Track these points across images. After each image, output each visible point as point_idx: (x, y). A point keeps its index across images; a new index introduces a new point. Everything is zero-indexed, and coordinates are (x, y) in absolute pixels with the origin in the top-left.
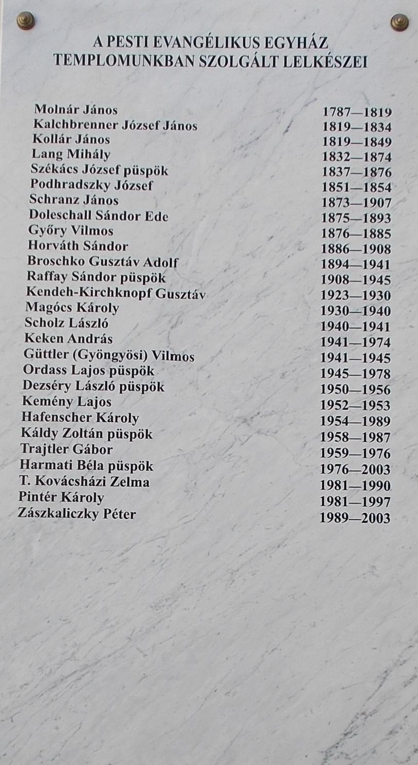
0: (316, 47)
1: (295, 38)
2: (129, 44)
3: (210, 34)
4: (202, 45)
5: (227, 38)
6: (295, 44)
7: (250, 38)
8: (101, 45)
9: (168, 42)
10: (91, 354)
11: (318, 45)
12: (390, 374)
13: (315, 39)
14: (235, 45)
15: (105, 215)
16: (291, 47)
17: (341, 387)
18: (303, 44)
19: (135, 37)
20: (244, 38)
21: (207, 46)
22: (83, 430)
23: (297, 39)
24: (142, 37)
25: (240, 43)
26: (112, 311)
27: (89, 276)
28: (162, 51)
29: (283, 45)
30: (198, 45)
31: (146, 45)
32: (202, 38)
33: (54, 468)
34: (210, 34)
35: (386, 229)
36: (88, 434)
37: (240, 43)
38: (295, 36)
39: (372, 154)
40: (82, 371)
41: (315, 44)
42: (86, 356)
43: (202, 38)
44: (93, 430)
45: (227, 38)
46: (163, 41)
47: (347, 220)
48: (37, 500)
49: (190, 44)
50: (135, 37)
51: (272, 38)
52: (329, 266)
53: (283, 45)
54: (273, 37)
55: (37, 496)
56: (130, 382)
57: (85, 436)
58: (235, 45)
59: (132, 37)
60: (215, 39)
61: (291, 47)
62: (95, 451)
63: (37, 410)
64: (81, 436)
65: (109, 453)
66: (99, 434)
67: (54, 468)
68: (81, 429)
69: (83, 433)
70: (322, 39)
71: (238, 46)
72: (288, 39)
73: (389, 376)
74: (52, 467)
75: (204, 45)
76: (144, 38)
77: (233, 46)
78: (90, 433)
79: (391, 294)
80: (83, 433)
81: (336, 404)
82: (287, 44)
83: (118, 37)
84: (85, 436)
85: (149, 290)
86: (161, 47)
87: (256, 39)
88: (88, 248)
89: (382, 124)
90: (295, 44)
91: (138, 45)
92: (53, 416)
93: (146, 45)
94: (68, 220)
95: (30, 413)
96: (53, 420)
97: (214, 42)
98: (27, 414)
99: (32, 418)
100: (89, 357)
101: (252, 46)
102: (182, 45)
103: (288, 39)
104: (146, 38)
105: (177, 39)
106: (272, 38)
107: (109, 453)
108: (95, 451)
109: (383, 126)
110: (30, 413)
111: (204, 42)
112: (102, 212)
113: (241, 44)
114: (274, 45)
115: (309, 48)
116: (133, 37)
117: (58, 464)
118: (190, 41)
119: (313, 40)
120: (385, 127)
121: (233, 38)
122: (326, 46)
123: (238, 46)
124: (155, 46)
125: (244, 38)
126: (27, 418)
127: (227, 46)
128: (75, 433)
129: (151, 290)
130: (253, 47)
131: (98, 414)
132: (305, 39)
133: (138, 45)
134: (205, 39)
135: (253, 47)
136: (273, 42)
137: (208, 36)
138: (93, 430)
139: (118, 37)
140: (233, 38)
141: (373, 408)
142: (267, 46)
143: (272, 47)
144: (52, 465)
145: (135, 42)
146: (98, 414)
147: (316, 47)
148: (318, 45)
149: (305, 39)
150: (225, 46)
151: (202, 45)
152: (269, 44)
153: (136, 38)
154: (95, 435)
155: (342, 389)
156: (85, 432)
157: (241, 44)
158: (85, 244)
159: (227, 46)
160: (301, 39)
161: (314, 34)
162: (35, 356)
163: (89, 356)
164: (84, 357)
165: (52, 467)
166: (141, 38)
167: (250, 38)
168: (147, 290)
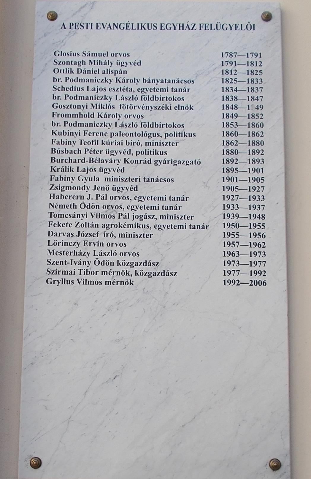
0: (189, 29)
1: (177, 24)
2: (82, 28)
3: (128, 22)
4: (124, 28)
5: (138, 24)
6: (177, 28)
7: (152, 24)
8: (65, 28)
9: (105, 26)
10: (85, 178)
11: (191, 28)
12: (265, 217)
13: (189, 25)
14: (143, 28)
15: (88, 54)
16: (175, 29)
17: (235, 225)
18: (182, 27)
19: (85, 23)
20: (148, 24)
21: (127, 29)
22: (87, 223)
23: (178, 25)
24: (89, 23)
25: (146, 27)
26: (109, 64)
27: (88, 71)
28: (97, 58)
29: (170, 28)
30: (122, 28)
31: (92, 28)
32: (124, 24)
33: (67, 274)
34: (128, 22)
35: (235, 168)
36: (90, 226)
37: (146, 27)
38: (177, 23)
39: (226, 106)
40: (83, 170)
41: (189, 28)
42: (83, 180)
43: (124, 24)
44: (93, 223)
45: (138, 24)
46: (101, 26)
47: (236, 82)
48: (63, 264)
49: (117, 28)
50: (85, 23)
51: (164, 24)
52: (226, 126)
53: (170, 28)
54: (165, 23)
55: (63, 262)
56: (113, 186)
57: (88, 227)
58: (143, 28)
59: (83, 24)
60: (131, 25)
61: (175, 29)
62: (88, 273)
63: (58, 193)
64: (86, 227)
65: (96, 274)
66: (97, 225)
67: (67, 274)
68: (86, 223)
69: (87, 225)
70: (193, 25)
71: (145, 29)
72: (173, 24)
73: (264, 218)
74: (66, 273)
75: (125, 28)
76: (90, 24)
77: (141, 29)
78: (91, 225)
79: (264, 143)
80: (87, 225)
81: (232, 244)
82: (173, 28)
83: (75, 24)
84: (88, 227)
85: (97, 232)
86: (100, 29)
87: (155, 25)
88: (85, 55)
89: (232, 88)
90: (177, 28)
91: (87, 28)
92: (61, 262)
93: (92, 28)
94: (61, 91)
95: (54, 194)
96: (60, 264)
97: (130, 26)
98: (52, 195)
99: (55, 197)
100: (84, 180)
101: (152, 29)
102: (112, 28)
103: (173, 24)
104: (92, 24)
105: (109, 25)
106: (164, 24)
107: (96, 274)
108: (88, 273)
109: (233, 89)
110: (54, 194)
111: (125, 26)
112: (86, 52)
113: (146, 28)
114: (165, 28)
115: (186, 30)
116: (84, 24)
117: (70, 272)
118: (117, 26)
119: (188, 25)
120: (233, 89)
121: (142, 24)
122: (195, 29)
123: (145, 29)
124: (97, 28)
125: (148, 24)
126: (52, 198)
127: (138, 29)
128: (82, 225)
129: (98, 233)
130: (153, 29)
131: (117, 78)
132: (183, 24)
133: (87, 28)
134: (125, 25)
135: (153, 29)
136: (165, 26)
137: (127, 23)
138: (93, 223)
139: (75, 24)
140: (142, 24)
141: (255, 237)
142: (161, 29)
143: (164, 29)
144: (66, 272)
145: (85, 26)
146: (117, 78)
147: (189, 29)
148: (191, 28)
149: (183, 24)
150: (137, 28)
151: (124, 28)
152: (162, 27)
153: (86, 24)
154: (94, 226)
155: (235, 225)
156: (88, 224)
157: (146, 28)
158: (83, 53)
159: (138, 29)
160: (181, 25)
161: (188, 22)
162: (58, 107)
163: (84, 180)
164: (81, 180)
165: (66, 273)
166: (88, 24)
167: (152, 24)
168: (97, 233)
